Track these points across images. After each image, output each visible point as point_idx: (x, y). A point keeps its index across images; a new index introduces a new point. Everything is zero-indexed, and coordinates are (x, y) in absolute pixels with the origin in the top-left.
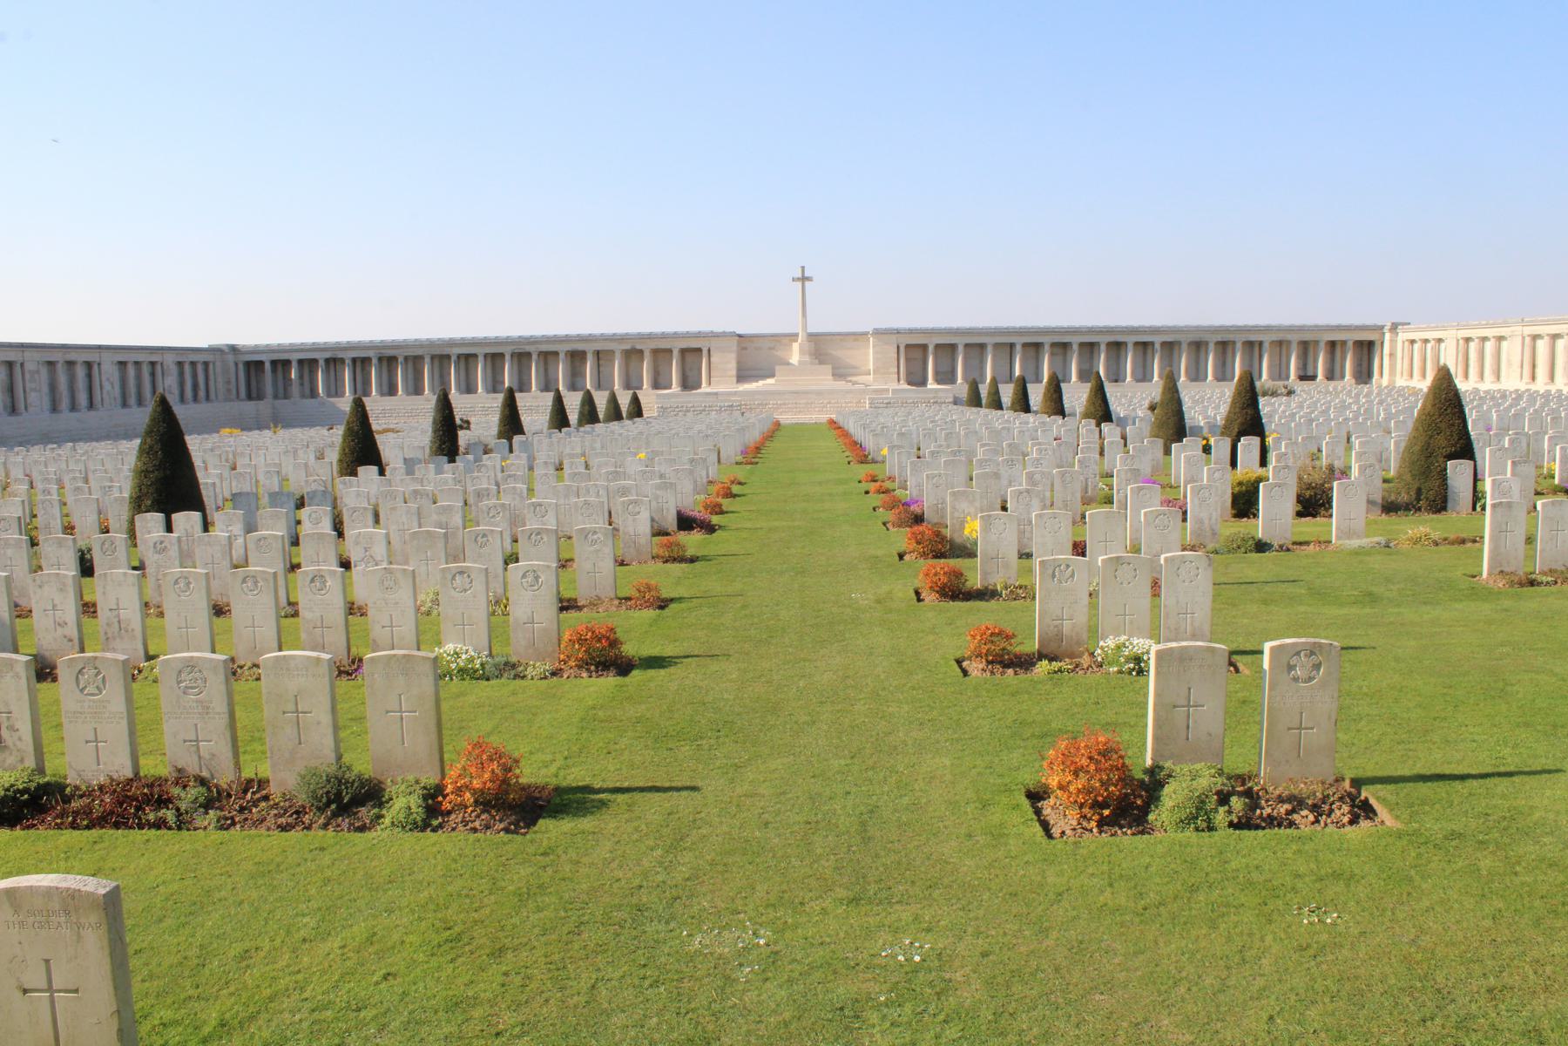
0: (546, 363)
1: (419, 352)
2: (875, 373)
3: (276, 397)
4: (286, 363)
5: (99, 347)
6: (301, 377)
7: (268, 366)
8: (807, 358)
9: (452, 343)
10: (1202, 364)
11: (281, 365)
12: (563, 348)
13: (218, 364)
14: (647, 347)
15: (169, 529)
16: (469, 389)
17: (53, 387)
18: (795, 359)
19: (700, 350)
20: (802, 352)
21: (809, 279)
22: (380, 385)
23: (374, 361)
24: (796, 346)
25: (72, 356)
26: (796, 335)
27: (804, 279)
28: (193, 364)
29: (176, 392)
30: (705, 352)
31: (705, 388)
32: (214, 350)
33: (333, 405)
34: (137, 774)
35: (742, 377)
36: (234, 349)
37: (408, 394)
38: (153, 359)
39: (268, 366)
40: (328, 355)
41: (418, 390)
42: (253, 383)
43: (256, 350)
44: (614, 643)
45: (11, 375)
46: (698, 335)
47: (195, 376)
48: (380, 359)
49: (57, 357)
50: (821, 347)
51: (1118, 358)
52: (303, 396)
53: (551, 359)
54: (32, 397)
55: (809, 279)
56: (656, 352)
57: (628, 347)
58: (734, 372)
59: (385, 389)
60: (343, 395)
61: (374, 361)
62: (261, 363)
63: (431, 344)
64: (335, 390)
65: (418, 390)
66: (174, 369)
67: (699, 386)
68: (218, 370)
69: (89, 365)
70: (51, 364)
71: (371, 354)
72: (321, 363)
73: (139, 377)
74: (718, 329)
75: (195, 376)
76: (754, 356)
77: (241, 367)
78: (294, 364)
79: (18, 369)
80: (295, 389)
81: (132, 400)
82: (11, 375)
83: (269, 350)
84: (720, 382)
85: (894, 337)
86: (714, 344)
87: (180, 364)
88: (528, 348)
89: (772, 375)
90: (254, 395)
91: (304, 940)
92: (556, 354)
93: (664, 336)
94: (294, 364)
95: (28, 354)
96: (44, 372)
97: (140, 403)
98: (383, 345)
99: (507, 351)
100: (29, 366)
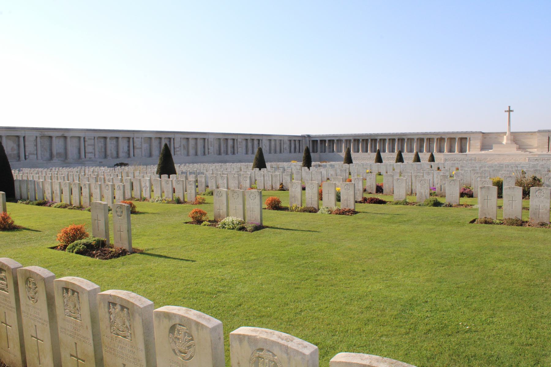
0: (440, 144)
1: (367, 138)
2: (538, 149)
3: (321, 152)
4: (325, 141)
5: (262, 135)
6: (329, 146)
7: (319, 142)
8: (509, 142)
9: (377, 135)
10: (225, 150)
11: (323, 141)
12: (416, 137)
13: (304, 141)
14: (446, 137)
15: (169, 178)
16: (440, 151)
17: (247, 146)
18: (505, 142)
19: (466, 138)
20: (507, 139)
21: (512, 111)
22: (389, 148)
23: (397, 140)
24: (505, 137)
25: (253, 138)
26: (506, 133)
27: (510, 111)
28: (295, 141)
29: (268, 148)
30: (468, 139)
31: (467, 152)
32: (303, 137)
33: (339, 155)
34: (261, 223)
35: (482, 149)
36: (309, 136)
37: (389, 152)
38: (280, 139)
39: (319, 142)
40: (337, 138)
41: (393, 151)
42: (315, 148)
43: (316, 137)
44: (279, 202)
45: (234, 143)
46: (466, 133)
47: (295, 145)
48: (399, 139)
49: (273, 138)
50: (517, 139)
51: (442, 144)
52: (330, 152)
53: (463, 141)
54: (239, 150)
55: (512, 111)
56: (346, 140)
57: (439, 137)
58: (479, 147)
59: (391, 150)
60: (341, 151)
61: (397, 140)
62: (317, 141)
63: (371, 135)
64: (340, 151)
65: (393, 151)
66: (288, 143)
67: (465, 152)
68: (304, 143)
69: (259, 140)
70: (247, 140)
71: (351, 138)
72: (335, 141)
73: (275, 145)
74: (474, 130)
75: (295, 145)
76: (488, 140)
77: (311, 142)
78: (327, 142)
79: (206, 141)
80: (327, 150)
81: (272, 151)
82: (234, 143)
83: (319, 136)
84: (474, 149)
85: (547, 133)
86: (472, 136)
87: (290, 141)
88: (404, 137)
89: (491, 149)
90: (315, 151)
91: (475, 272)
92: (455, 139)
93: (453, 133)
94: (327, 142)
95: (239, 137)
96: (244, 143)
97: (253, 153)
98: (355, 135)
99: (396, 138)
100: (239, 140)
